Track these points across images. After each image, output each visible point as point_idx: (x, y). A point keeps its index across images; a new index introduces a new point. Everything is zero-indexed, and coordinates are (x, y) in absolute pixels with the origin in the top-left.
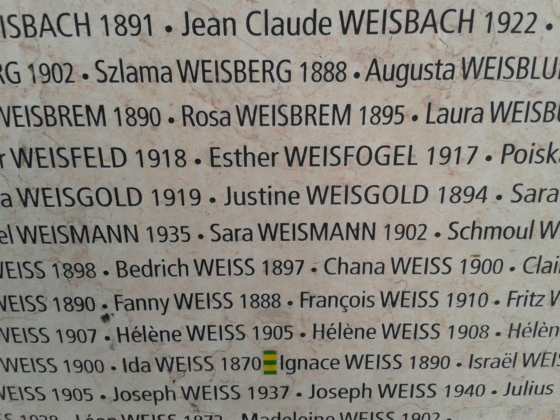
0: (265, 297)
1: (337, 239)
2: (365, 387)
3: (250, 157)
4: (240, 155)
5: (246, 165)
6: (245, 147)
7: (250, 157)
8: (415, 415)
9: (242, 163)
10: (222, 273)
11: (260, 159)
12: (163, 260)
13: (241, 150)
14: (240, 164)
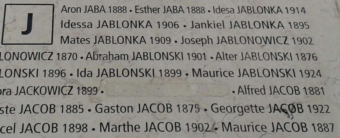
0: (198, 8)
1: (90, 12)
2: (110, 54)
3: (130, 127)
4: (125, 126)
5: (128, 131)
6: (128, 122)
7: (130, 127)
8: (64, 76)
9: (126, 130)
10: (308, 54)
11: (135, 128)
12: (220, 69)
13: (126, 124)
14: (125, 131)
